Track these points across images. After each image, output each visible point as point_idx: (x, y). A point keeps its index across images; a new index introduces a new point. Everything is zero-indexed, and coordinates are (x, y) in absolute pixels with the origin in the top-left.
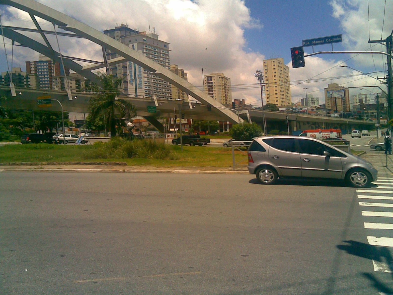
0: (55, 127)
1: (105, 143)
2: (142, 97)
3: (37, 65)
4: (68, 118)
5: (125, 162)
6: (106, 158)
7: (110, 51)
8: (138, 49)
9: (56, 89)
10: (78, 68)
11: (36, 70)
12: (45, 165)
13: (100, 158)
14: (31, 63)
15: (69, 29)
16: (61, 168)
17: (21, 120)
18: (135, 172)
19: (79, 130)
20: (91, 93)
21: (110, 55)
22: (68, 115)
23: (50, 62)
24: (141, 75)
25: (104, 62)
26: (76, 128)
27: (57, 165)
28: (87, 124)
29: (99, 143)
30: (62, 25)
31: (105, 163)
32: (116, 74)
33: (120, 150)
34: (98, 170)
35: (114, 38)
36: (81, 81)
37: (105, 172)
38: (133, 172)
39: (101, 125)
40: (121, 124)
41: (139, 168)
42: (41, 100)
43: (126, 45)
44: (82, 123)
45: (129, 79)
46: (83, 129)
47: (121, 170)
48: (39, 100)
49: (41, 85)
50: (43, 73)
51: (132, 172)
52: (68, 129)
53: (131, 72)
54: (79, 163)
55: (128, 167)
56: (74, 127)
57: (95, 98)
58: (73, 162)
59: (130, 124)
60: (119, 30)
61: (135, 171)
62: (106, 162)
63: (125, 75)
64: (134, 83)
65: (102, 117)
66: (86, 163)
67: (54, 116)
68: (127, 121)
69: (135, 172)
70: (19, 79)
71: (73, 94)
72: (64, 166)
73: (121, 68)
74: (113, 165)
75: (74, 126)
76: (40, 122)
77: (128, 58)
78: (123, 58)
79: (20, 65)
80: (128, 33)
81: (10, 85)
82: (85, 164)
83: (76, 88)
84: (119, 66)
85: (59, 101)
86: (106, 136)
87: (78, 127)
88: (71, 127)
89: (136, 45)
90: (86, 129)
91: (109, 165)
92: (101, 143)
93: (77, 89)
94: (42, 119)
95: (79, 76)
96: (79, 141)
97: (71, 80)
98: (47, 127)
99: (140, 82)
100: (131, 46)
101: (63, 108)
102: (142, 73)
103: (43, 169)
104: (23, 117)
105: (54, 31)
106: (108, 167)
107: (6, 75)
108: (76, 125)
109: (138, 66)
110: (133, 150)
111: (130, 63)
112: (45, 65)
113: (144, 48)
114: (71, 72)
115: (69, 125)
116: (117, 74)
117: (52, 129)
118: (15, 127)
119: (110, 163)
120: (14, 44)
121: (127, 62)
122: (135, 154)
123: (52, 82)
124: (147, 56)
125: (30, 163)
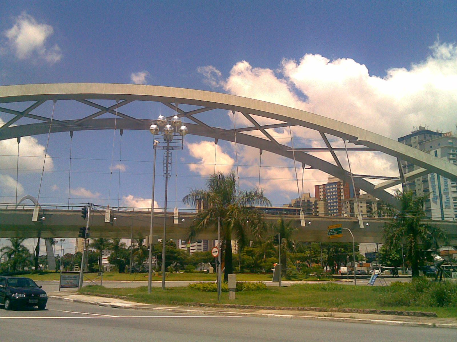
0: (344, 262)
1: (405, 284)
2: (452, 220)
3: (326, 188)
4: (359, 250)
5: (435, 313)
6: (409, 306)
7: (406, 162)
8: (442, 156)
9: (345, 215)
10: (369, 188)
11: (324, 195)
12: (335, 311)
13: (401, 305)
14: (320, 187)
15: (360, 143)
16: (353, 316)
17: (309, 254)
18: (449, 328)
19: (371, 266)
20: (386, 217)
21: (407, 167)
22: (359, 247)
23: (339, 184)
24: (447, 189)
25: (400, 177)
26: (367, 263)
27: (348, 313)
28: (381, 258)
29: (397, 284)
30: (353, 139)
31: (408, 313)
32: (414, 191)
33: (426, 296)
34: (400, 322)
35: (411, 146)
36: (373, 203)
37: (409, 326)
38: (447, 328)
39: (397, 259)
40: (426, 258)
41: (454, 321)
42: (332, 230)
43: (426, 152)
44: (374, 257)
45: (431, 196)
46: (375, 265)
47: (430, 324)
48: (330, 230)
49: (329, 212)
50: (331, 197)
51: (445, 328)
52: (358, 264)
53: (433, 187)
54: (375, 311)
55: (439, 319)
56: (364, 262)
57: (391, 224)
58: (368, 310)
59: (438, 257)
60: (417, 135)
61: (449, 326)
62: (409, 311)
63: (426, 190)
64: (438, 201)
65: (399, 248)
66: (384, 312)
67: (343, 248)
68: (434, 254)
69: (449, 328)
70: (308, 206)
71: (364, 221)
72: (357, 314)
73: (421, 182)
74: (419, 316)
75: (364, 261)
76: (327, 256)
77: (430, 169)
78: (425, 170)
79: (309, 190)
80: (428, 137)
81: (299, 215)
82: (383, 313)
83: (368, 212)
84: (418, 180)
85: (350, 230)
86: (404, 273)
87: (370, 262)
88: (361, 262)
89: (439, 151)
90: (379, 264)
91: (414, 316)
92: (400, 284)
93: (368, 214)
94: (330, 252)
95: (371, 197)
96: (372, 281)
97: (361, 203)
98: (335, 262)
99: (446, 198)
100: (433, 152)
101: (353, 238)
102: (449, 187)
103: (334, 317)
104: (310, 251)
105: (345, 147)
106: (411, 319)
107: (295, 202)
108: (367, 259)
109: (443, 177)
110: (445, 295)
111: (432, 175)
112: (334, 188)
113: (450, 154)
114: (362, 192)
115: (359, 259)
116: (415, 191)
117: (341, 264)
118: (303, 262)
119: (415, 313)
120: (305, 167)
121: (428, 175)
122: (447, 301)
123: (341, 206)
124: (454, 163)
125: (319, 308)
